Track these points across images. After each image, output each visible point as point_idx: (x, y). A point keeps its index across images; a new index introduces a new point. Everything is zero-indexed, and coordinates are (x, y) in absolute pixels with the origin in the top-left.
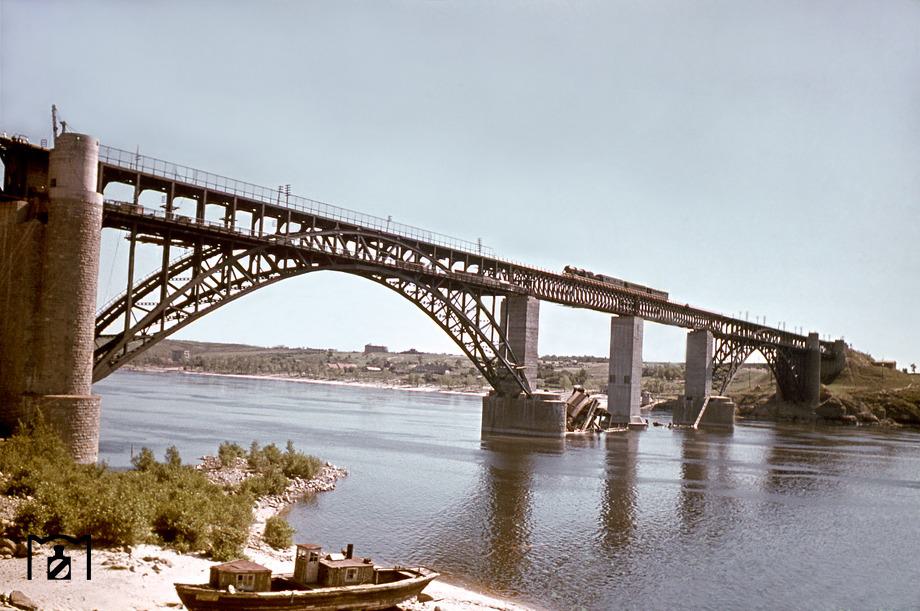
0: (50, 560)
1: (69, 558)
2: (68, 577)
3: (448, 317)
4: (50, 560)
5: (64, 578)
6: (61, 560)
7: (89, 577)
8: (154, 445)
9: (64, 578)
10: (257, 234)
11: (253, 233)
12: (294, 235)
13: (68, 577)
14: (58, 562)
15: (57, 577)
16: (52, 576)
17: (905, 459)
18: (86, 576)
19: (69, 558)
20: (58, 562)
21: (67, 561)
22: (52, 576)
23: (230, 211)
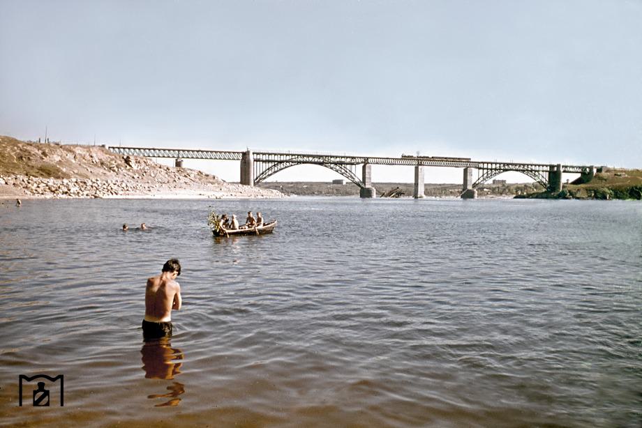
4: (35, 392)
6: (42, 393)
15: (40, 404)
16: (36, 404)
21: (47, 393)
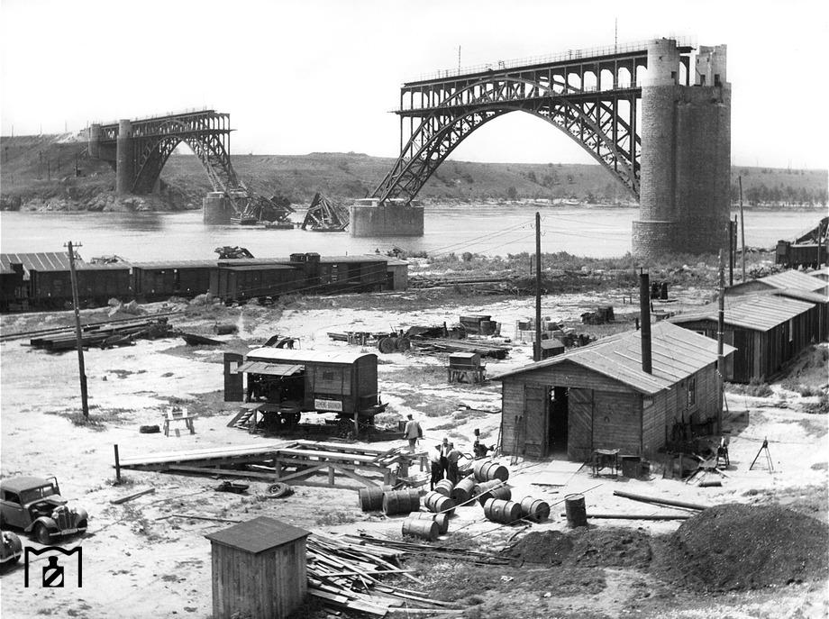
0: (45, 569)
1: (62, 568)
2: (61, 585)
3: (582, 133)
5: (58, 586)
7: (80, 585)
8: (712, 72)
9: (58, 586)
10: (431, 106)
11: (423, 106)
12: (490, 92)
13: (61, 585)
14: (52, 571)
16: (47, 584)
17: (322, 298)
18: (77, 584)
19: (62, 568)
20: (52, 571)
22: (47, 584)
23: (632, 318)
